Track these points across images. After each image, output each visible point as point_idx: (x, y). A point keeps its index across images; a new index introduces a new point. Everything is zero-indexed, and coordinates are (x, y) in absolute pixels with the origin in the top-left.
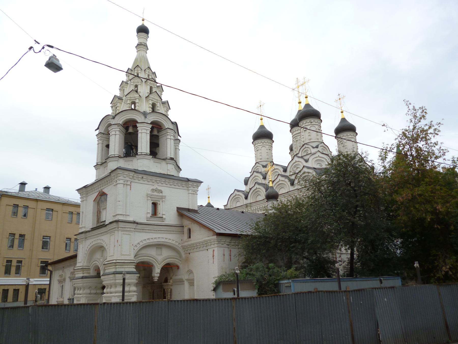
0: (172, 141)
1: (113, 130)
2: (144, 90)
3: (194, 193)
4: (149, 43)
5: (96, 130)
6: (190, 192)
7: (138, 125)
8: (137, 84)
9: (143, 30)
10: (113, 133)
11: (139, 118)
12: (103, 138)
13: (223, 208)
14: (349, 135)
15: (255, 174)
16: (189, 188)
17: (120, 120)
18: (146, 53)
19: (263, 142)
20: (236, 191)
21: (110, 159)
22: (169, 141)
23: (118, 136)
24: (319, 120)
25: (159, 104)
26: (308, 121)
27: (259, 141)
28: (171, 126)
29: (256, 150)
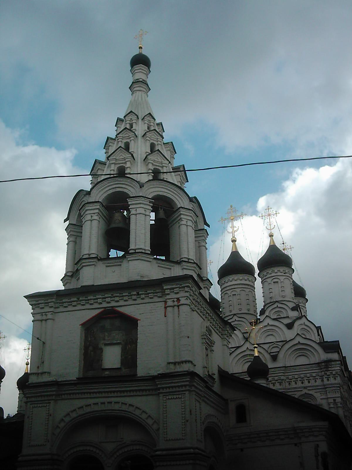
0: (190, 229)
2: (140, 148)
8: (128, 141)
9: (140, 61)
11: (132, 191)
12: (75, 234)
17: (99, 195)
21: (85, 263)
22: (183, 228)
23: (95, 223)
24: (303, 299)
28: (189, 205)
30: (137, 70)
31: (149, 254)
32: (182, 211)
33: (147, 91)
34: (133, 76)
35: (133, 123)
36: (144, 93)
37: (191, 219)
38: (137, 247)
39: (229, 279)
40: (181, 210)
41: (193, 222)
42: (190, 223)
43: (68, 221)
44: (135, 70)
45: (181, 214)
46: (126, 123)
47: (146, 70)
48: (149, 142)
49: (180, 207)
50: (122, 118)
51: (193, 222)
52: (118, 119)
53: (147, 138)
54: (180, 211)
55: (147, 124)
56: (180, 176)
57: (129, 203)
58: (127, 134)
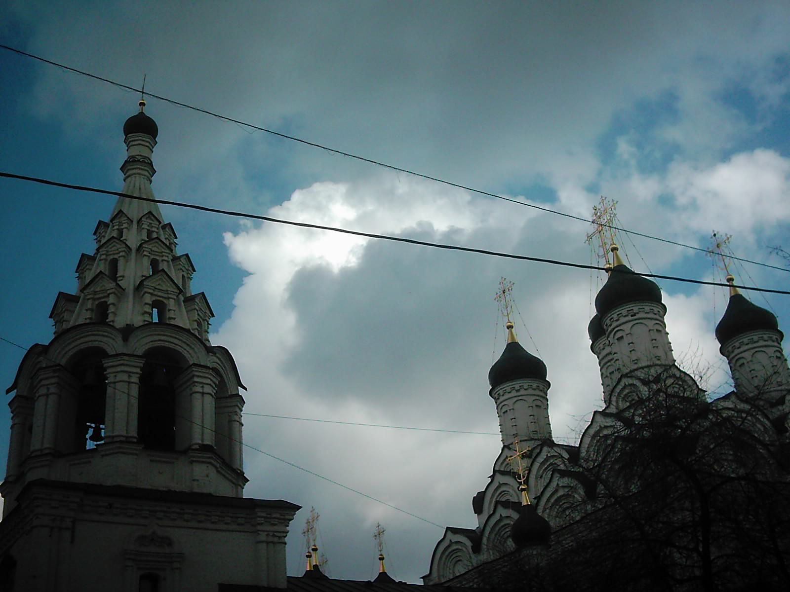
1: (43, 382)
3: (276, 540)
4: (157, 158)
5: (8, 391)
6: (263, 536)
7: (107, 363)
10: (43, 391)
11: (113, 344)
13: (421, 583)
14: (755, 338)
15: (500, 479)
16: (259, 528)
18: (151, 182)
19: (517, 387)
20: (449, 533)
23: (52, 399)
25: (172, 302)
26: (624, 312)
27: (507, 386)
29: (502, 413)
30: (133, 141)
31: (134, 443)
32: (196, 371)
33: (150, 174)
34: (127, 150)
35: (123, 229)
36: (144, 178)
37: (209, 381)
38: (116, 433)
39: (611, 317)
40: (194, 369)
41: (213, 387)
42: (208, 389)
43: (16, 390)
44: (130, 141)
45: (194, 376)
46: (113, 229)
47: (149, 140)
48: (149, 259)
49: (192, 364)
50: (107, 220)
51: (213, 387)
52: (100, 222)
53: (145, 253)
54: (193, 371)
55: (146, 231)
56: (197, 311)
57: (105, 365)
58: (114, 246)
